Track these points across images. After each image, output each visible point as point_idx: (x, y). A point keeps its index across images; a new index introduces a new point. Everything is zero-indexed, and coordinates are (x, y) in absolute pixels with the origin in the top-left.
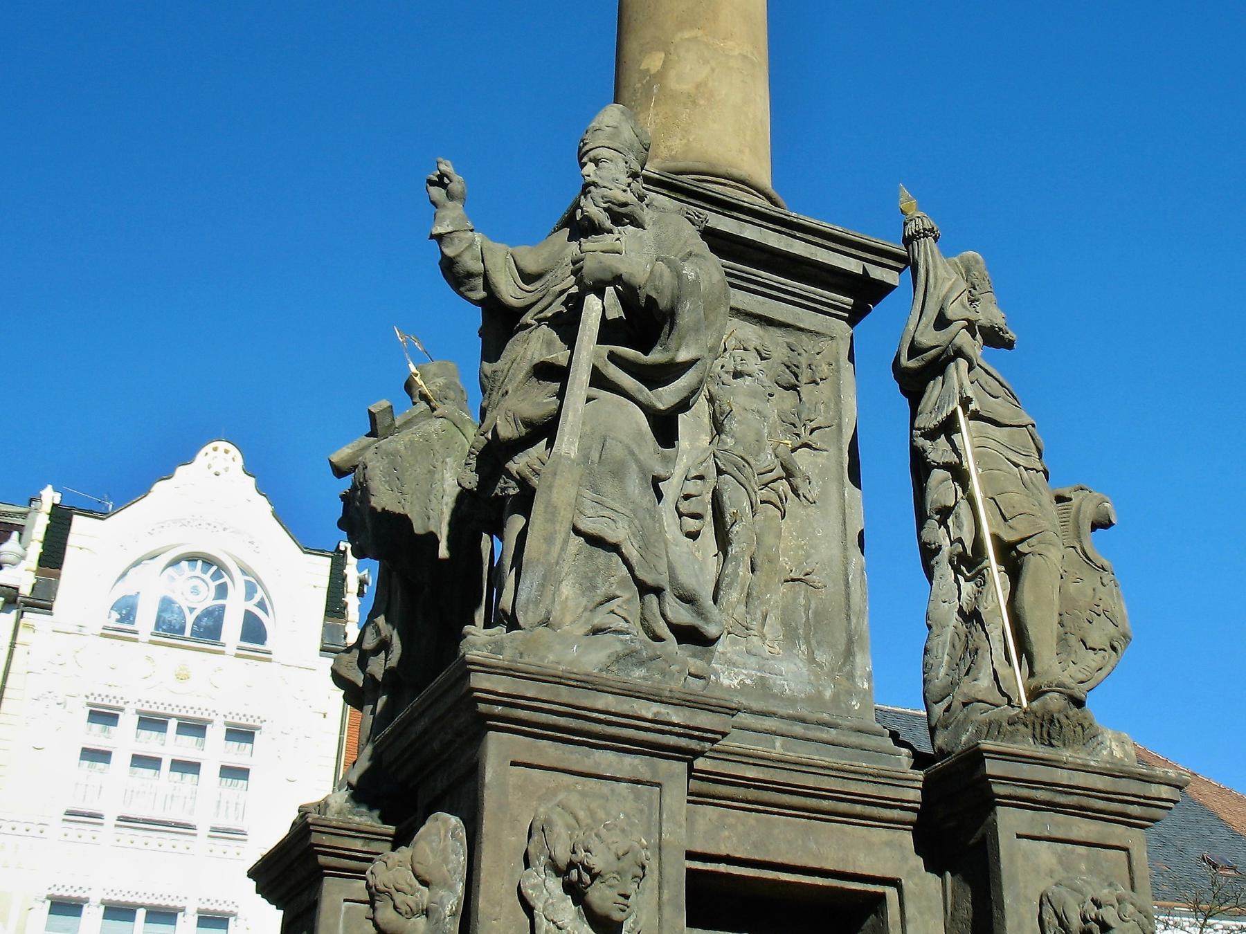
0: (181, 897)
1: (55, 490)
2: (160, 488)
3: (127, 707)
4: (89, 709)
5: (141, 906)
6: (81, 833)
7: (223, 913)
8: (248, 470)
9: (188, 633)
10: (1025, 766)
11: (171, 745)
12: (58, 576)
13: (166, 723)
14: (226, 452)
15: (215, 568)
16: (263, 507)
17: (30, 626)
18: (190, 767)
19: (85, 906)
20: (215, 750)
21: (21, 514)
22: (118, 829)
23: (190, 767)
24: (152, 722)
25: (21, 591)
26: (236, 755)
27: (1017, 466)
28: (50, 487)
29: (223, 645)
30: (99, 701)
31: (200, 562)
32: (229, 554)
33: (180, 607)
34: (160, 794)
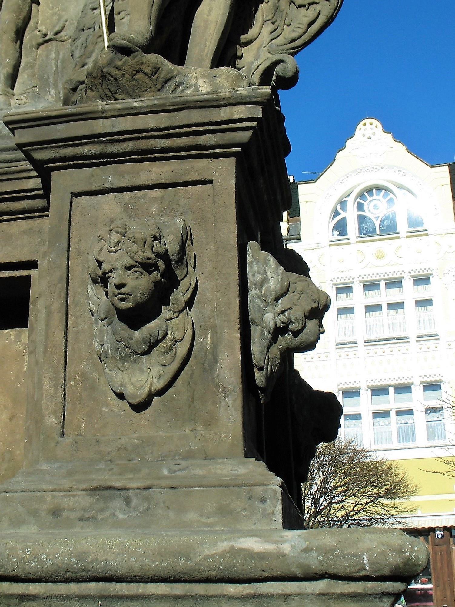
4: (335, 287)
9: (378, 232)
13: (379, 284)
14: (371, 124)
15: (383, 191)
29: (398, 233)
30: (339, 281)
33: (370, 219)
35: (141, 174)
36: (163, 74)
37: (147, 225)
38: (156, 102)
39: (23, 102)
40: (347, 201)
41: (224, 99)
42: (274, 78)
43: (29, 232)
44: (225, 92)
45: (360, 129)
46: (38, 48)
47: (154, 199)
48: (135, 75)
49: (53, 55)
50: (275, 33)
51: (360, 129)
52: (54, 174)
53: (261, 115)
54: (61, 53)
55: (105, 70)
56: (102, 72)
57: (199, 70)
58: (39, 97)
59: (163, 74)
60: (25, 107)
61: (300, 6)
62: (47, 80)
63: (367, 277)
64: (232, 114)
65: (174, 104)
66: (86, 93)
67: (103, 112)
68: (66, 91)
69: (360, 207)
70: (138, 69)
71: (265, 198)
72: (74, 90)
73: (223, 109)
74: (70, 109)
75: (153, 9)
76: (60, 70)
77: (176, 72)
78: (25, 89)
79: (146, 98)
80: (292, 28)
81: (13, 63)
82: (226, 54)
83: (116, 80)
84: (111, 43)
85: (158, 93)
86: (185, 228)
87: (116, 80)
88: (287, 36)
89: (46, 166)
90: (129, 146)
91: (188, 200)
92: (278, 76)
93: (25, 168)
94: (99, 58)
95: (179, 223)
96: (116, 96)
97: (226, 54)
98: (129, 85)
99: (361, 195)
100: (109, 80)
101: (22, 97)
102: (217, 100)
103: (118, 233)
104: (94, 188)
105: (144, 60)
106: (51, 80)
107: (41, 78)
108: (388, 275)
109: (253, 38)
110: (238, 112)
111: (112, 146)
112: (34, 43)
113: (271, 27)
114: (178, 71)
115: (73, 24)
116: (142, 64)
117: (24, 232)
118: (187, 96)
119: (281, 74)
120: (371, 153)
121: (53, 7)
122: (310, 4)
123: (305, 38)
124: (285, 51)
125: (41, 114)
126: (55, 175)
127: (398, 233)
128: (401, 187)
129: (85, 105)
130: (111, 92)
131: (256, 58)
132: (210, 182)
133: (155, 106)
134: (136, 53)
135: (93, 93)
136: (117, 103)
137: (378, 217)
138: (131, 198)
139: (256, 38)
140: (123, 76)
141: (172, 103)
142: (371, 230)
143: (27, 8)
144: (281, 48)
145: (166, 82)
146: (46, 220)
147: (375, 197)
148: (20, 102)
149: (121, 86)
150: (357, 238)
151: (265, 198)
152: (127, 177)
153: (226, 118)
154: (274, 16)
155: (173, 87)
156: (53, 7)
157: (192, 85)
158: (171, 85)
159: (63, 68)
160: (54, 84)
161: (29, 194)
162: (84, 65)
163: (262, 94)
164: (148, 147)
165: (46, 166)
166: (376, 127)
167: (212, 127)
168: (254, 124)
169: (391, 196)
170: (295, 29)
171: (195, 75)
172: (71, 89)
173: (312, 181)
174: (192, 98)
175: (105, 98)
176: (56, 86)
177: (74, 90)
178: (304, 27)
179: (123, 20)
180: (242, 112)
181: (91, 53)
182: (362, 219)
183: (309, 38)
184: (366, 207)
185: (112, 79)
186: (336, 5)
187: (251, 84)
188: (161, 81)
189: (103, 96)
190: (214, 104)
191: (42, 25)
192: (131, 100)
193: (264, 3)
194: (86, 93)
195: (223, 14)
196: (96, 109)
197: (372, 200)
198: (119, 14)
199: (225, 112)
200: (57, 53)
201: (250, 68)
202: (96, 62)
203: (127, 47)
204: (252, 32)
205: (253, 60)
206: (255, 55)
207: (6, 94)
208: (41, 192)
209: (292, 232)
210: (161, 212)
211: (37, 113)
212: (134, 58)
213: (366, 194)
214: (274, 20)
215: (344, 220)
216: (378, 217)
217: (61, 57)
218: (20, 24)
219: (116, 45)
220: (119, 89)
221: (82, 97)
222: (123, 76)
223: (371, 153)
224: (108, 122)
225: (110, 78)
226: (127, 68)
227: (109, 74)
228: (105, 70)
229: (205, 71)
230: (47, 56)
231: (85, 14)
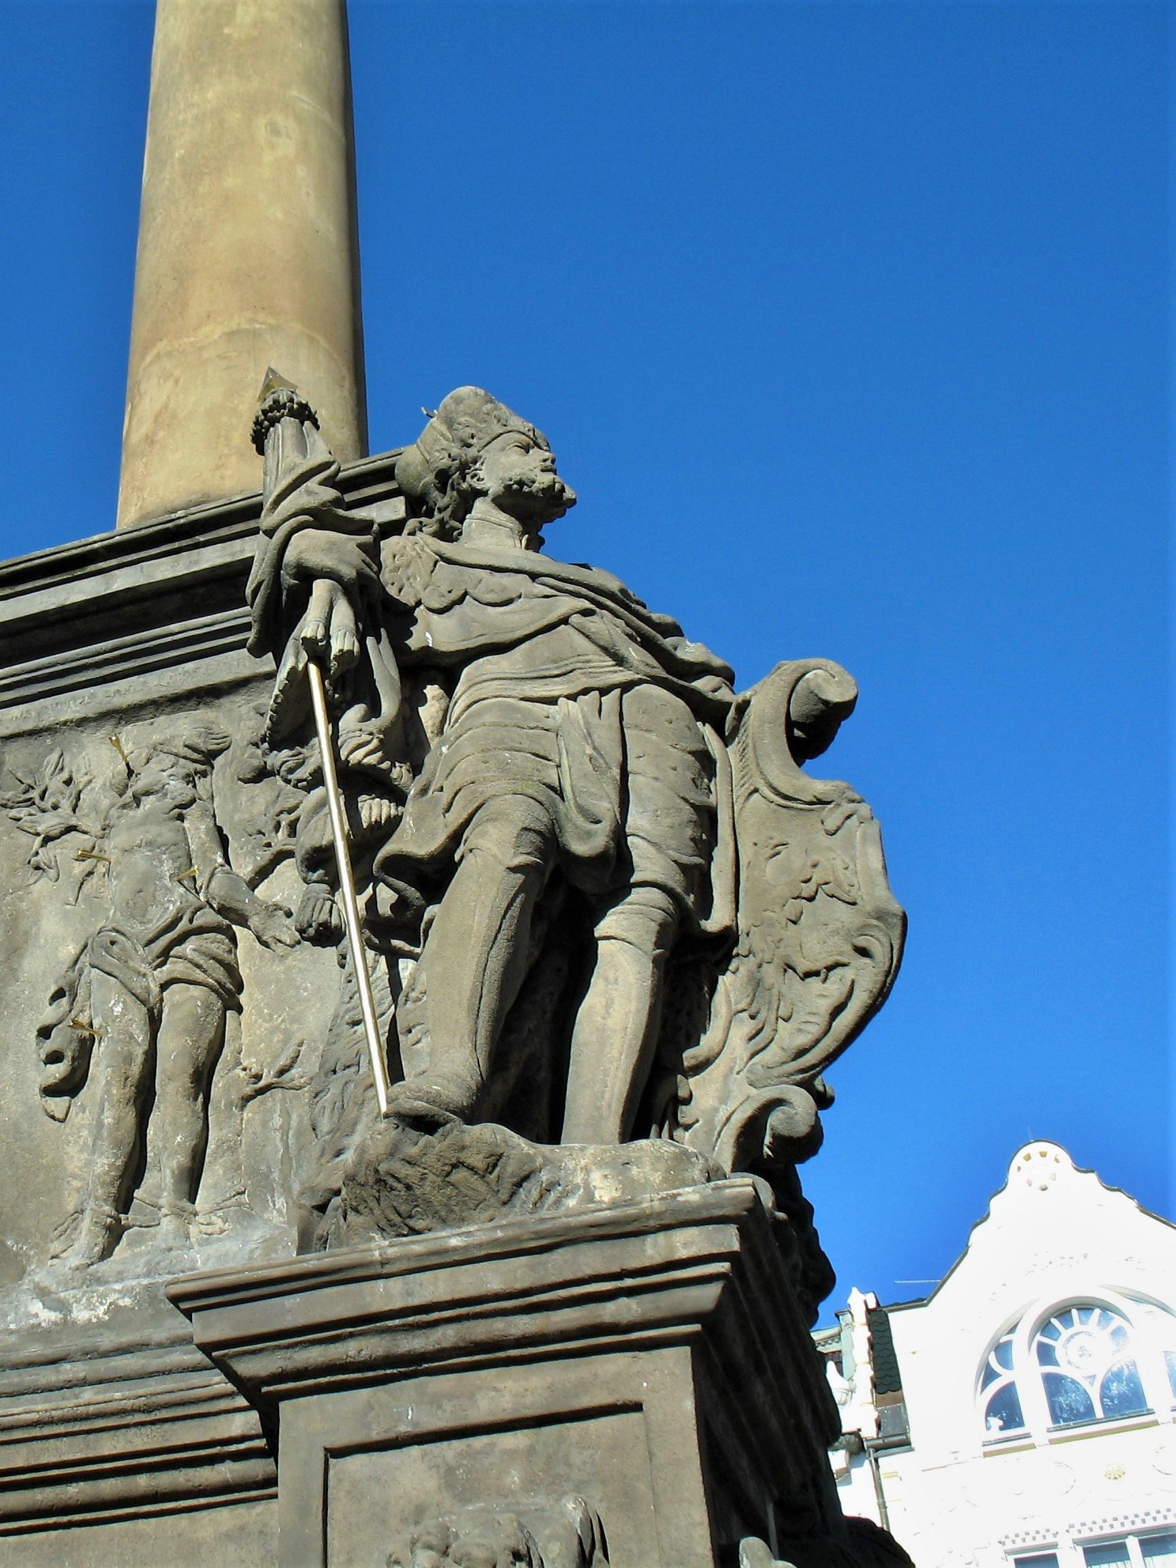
1: (864, 1292)
2: (978, 1237)
4: (1011, 1558)
8: (1082, 1165)
9: (1099, 1413)
10: (435, 1262)
12: (902, 1400)
13: (1123, 1547)
14: (1043, 1155)
15: (1097, 1312)
16: (1123, 1204)
17: (893, 1475)
21: (832, 1337)
25: (863, 1434)
27: (552, 701)
28: (854, 1290)
29: (1151, 1412)
30: (1019, 1544)
31: (1074, 1312)
32: (1107, 1287)
33: (1073, 1382)
35: (478, 1397)
36: (510, 1168)
37: (496, 1525)
38: (500, 1234)
39: (216, 1228)
40: (1009, 1343)
41: (649, 1217)
42: (768, 1140)
43: (236, 1536)
44: (650, 1202)
45: (1019, 1169)
46: (243, 1107)
47: (512, 1455)
48: (448, 1174)
49: (277, 1121)
50: (758, 1040)
51: (1019, 1169)
52: (285, 1407)
53: (736, 1246)
54: (294, 1116)
55: (383, 1168)
56: (377, 1171)
57: (591, 1150)
58: (251, 1216)
59: (510, 1168)
60: (221, 1240)
61: (808, 975)
62: (267, 1176)
63: (1091, 1530)
64: (672, 1248)
65: (539, 1235)
66: (345, 1218)
67: (383, 1264)
68: (305, 1213)
69: (1046, 1355)
70: (454, 1161)
71: (774, 1424)
72: (322, 1208)
73: (650, 1239)
74: (313, 1261)
75: (480, 1021)
76: (293, 1151)
77: (539, 1161)
78: (219, 1200)
79: (476, 1227)
80: (796, 1026)
81: (190, 1144)
82: (652, 1105)
83: (408, 1187)
84: (393, 1107)
85: (505, 1209)
86: (588, 1522)
87: (408, 1187)
88: (786, 1044)
89: (265, 1389)
90: (446, 1336)
91: (591, 1451)
92: (775, 1137)
93: (217, 1392)
94: (369, 1142)
95: (572, 1510)
96: (411, 1223)
97: (652, 1105)
98: (437, 1198)
99: (1044, 1326)
100: (392, 1189)
101: (214, 1218)
102: (636, 1219)
103: (429, 1547)
104: (375, 1435)
105: (467, 1140)
106: (276, 1175)
107: (253, 1172)
108: (1144, 1521)
109: (712, 1053)
110: (685, 1243)
111: (410, 1337)
112: (235, 1097)
113: (748, 1026)
114: (544, 1157)
115: (316, 1049)
116: (463, 1148)
117: (228, 1537)
118: (567, 1216)
119: (784, 1130)
120: (1050, 1219)
121: (271, 1016)
122: (830, 968)
123: (828, 1044)
124: (785, 1079)
125: (248, 1276)
126: (286, 1408)
127: (1151, 1412)
128: (1139, 1299)
129: (344, 1250)
130: (400, 1215)
131: (724, 1100)
132: (637, 1407)
133: (495, 1242)
134: (448, 1126)
135: (361, 1219)
136: (413, 1242)
137: (1094, 1377)
138: (461, 1455)
139: (719, 1054)
140: (423, 1178)
141: (536, 1233)
142: (1082, 1409)
143: (214, 1020)
144: (776, 1072)
145: (519, 1185)
146: (273, 1505)
147: (1077, 1326)
148: (210, 1229)
149: (420, 1201)
150: (1049, 1431)
151: (774, 1424)
152: (448, 1406)
153: (658, 1260)
154: (752, 1001)
155: (535, 1194)
156: (271, 1016)
157: (577, 1187)
158: (531, 1191)
159: (301, 1148)
160: (282, 1186)
161: (233, 1448)
162: (339, 1153)
163: (735, 1197)
164: (491, 1336)
165: (265, 1389)
166: (1057, 1160)
167: (629, 1282)
168: (723, 1267)
169: (1117, 1321)
170: (803, 1027)
171: (583, 1162)
172: (313, 1207)
173: (920, 1301)
174: (580, 1219)
175: (388, 1229)
176: (287, 1190)
177: (322, 1208)
178: (822, 1020)
179: (419, 1046)
180: (692, 1243)
181: (355, 1124)
182: (1054, 1384)
183: (835, 1044)
184: (1059, 1354)
185: (399, 1186)
186: (887, 964)
187: (712, 1174)
188: (508, 1183)
189: (383, 1223)
190: (629, 1228)
191: (249, 1056)
192: (444, 1234)
193: (728, 973)
194: (345, 1218)
195: (638, 1011)
196: (366, 1257)
197: (1072, 1337)
198: (410, 1031)
199: (655, 1245)
200: (286, 1114)
201: (710, 1122)
202: (362, 1150)
203: (426, 1116)
204: (709, 1040)
205: (716, 1103)
206: (719, 1095)
207: (179, 1213)
208: (261, 1443)
209: (888, 1428)
210: (530, 1485)
211: (239, 1272)
212: (445, 1136)
213: (1054, 1321)
214: (753, 1010)
215: (1009, 1389)
216: (1094, 1377)
217: (294, 1123)
218: (201, 1058)
219: (403, 1112)
220: (417, 1206)
221: (338, 1227)
222: (423, 1178)
223: (1050, 1219)
224: (396, 1284)
225: (396, 1184)
226: (430, 1159)
227: (393, 1176)
228: (383, 1168)
229: (605, 1151)
230: (264, 1124)
231: (337, 1035)
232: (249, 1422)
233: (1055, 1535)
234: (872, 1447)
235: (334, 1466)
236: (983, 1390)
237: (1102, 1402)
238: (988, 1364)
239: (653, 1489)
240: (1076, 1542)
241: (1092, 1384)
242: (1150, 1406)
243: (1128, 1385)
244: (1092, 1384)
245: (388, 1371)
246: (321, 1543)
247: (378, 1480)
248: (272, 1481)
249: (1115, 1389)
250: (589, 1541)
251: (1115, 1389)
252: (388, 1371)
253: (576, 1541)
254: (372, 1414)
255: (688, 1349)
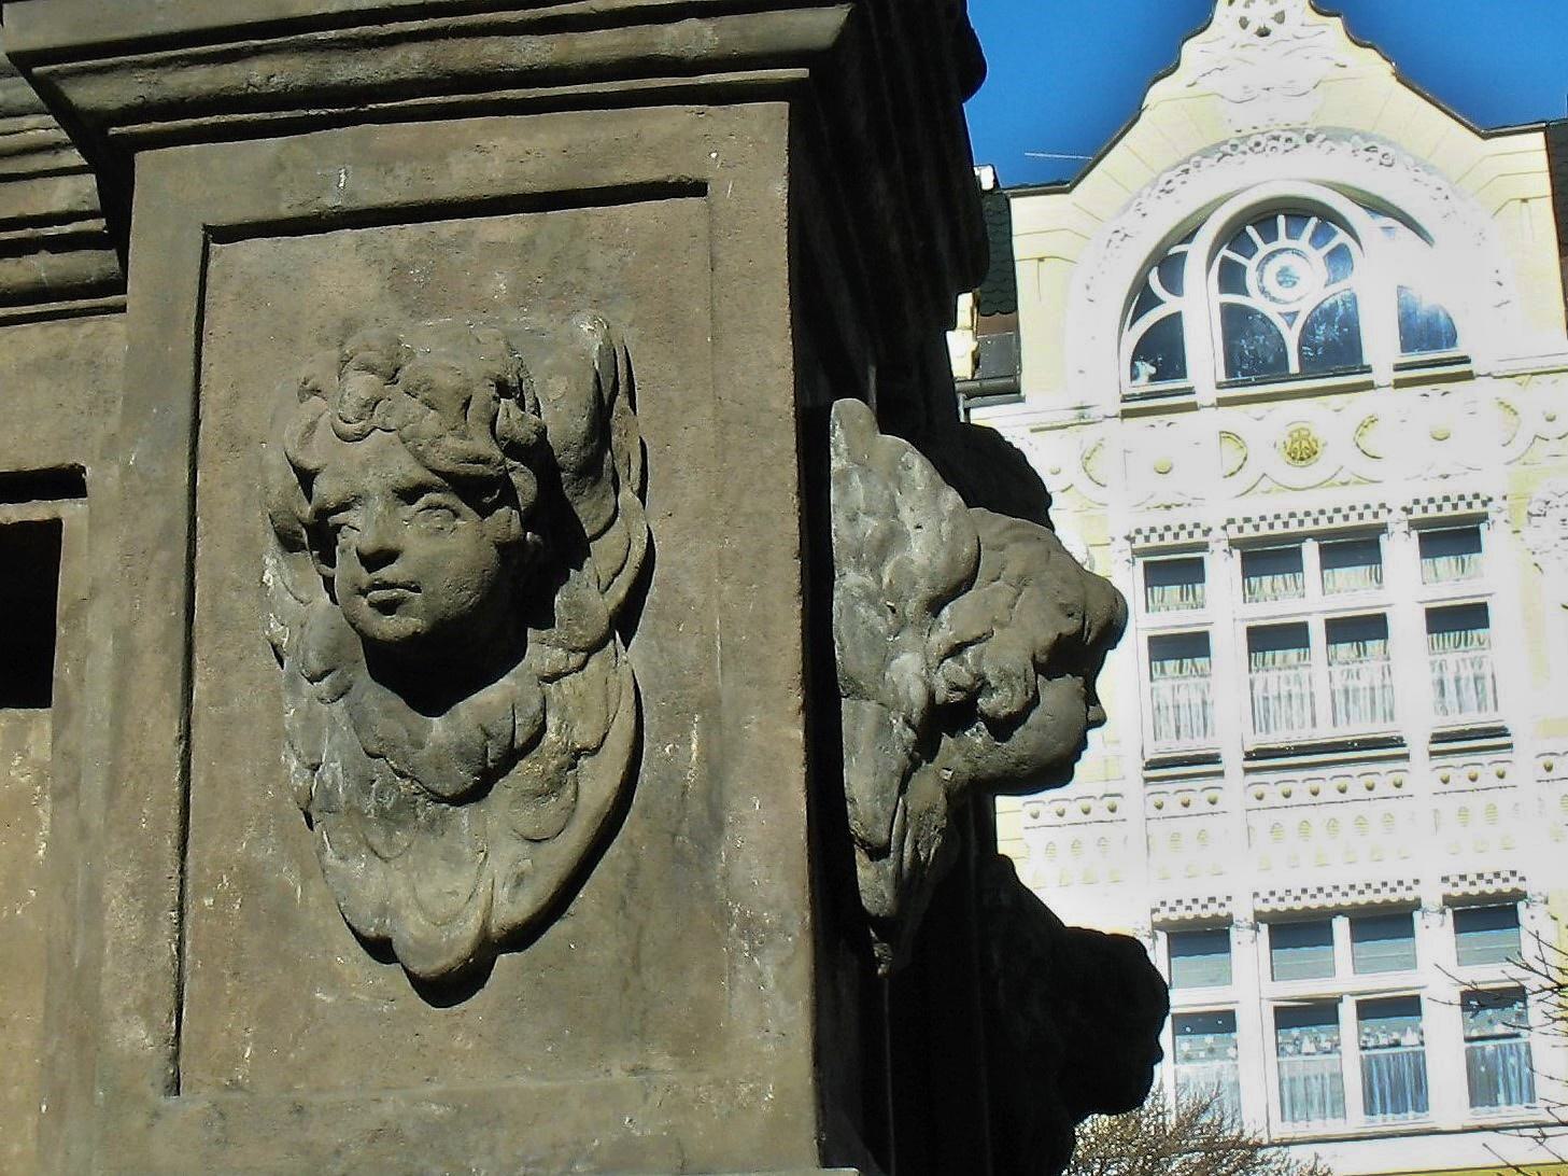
0: (1408, 882)
3: (1491, 509)
4: (1140, 562)
5: (1339, 911)
6: (1315, 785)
7: (1499, 896)
9: (1294, 367)
11: (1315, 594)
13: (1298, 552)
15: (1314, 221)
18: (1362, 629)
19: (1417, 915)
20: (1405, 583)
22: (1153, 787)
23: (1362, 629)
24: (1267, 556)
26: (1451, 582)
33: (1265, 319)
34: (1318, 692)
37: (473, 343)
40: (1183, 255)
43: (52, 366)
47: (496, 250)
52: (144, 160)
69: (1231, 278)
71: (894, 243)
86: (609, 353)
89: (114, 130)
91: (620, 251)
95: (587, 333)
104: (285, 209)
117: (39, 368)
127: (1368, 370)
128: (1376, 206)
132: (698, 189)
137: (1295, 314)
138: (418, 246)
142: (1271, 359)
146: (114, 322)
150: (1219, 386)
151: (894, 243)
152: (403, 172)
161: (54, 231)
165: (114, 130)
173: (1061, 182)
182: (1237, 321)
210: (524, 296)
213: (1250, 230)
215: (1175, 320)
216: (1295, 314)
232: (79, 191)
233: (1207, 532)
234: (963, 392)
235: (218, 254)
236: (1133, 322)
237: (1300, 351)
238: (1147, 284)
239: (713, 310)
240: (1233, 544)
241: (1290, 325)
242: (1366, 361)
243: (1340, 330)
244: (1290, 325)
245: (313, 112)
246: (192, 368)
247: (286, 280)
248: (118, 284)
249: (1321, 333)
250: (611, 380)
251: (1321, 333)
252: (313, 112)
253: (591, 380)
254: (281, 177)
255: (785, 105)
